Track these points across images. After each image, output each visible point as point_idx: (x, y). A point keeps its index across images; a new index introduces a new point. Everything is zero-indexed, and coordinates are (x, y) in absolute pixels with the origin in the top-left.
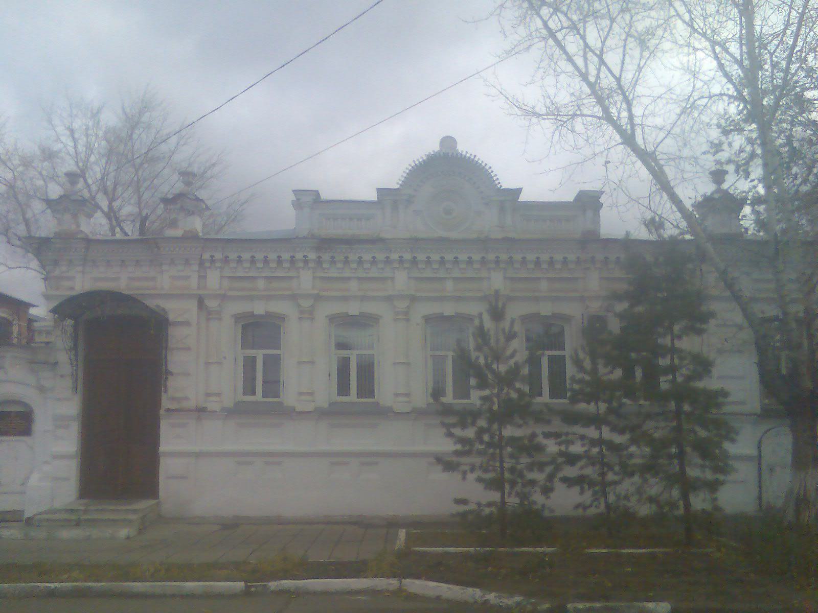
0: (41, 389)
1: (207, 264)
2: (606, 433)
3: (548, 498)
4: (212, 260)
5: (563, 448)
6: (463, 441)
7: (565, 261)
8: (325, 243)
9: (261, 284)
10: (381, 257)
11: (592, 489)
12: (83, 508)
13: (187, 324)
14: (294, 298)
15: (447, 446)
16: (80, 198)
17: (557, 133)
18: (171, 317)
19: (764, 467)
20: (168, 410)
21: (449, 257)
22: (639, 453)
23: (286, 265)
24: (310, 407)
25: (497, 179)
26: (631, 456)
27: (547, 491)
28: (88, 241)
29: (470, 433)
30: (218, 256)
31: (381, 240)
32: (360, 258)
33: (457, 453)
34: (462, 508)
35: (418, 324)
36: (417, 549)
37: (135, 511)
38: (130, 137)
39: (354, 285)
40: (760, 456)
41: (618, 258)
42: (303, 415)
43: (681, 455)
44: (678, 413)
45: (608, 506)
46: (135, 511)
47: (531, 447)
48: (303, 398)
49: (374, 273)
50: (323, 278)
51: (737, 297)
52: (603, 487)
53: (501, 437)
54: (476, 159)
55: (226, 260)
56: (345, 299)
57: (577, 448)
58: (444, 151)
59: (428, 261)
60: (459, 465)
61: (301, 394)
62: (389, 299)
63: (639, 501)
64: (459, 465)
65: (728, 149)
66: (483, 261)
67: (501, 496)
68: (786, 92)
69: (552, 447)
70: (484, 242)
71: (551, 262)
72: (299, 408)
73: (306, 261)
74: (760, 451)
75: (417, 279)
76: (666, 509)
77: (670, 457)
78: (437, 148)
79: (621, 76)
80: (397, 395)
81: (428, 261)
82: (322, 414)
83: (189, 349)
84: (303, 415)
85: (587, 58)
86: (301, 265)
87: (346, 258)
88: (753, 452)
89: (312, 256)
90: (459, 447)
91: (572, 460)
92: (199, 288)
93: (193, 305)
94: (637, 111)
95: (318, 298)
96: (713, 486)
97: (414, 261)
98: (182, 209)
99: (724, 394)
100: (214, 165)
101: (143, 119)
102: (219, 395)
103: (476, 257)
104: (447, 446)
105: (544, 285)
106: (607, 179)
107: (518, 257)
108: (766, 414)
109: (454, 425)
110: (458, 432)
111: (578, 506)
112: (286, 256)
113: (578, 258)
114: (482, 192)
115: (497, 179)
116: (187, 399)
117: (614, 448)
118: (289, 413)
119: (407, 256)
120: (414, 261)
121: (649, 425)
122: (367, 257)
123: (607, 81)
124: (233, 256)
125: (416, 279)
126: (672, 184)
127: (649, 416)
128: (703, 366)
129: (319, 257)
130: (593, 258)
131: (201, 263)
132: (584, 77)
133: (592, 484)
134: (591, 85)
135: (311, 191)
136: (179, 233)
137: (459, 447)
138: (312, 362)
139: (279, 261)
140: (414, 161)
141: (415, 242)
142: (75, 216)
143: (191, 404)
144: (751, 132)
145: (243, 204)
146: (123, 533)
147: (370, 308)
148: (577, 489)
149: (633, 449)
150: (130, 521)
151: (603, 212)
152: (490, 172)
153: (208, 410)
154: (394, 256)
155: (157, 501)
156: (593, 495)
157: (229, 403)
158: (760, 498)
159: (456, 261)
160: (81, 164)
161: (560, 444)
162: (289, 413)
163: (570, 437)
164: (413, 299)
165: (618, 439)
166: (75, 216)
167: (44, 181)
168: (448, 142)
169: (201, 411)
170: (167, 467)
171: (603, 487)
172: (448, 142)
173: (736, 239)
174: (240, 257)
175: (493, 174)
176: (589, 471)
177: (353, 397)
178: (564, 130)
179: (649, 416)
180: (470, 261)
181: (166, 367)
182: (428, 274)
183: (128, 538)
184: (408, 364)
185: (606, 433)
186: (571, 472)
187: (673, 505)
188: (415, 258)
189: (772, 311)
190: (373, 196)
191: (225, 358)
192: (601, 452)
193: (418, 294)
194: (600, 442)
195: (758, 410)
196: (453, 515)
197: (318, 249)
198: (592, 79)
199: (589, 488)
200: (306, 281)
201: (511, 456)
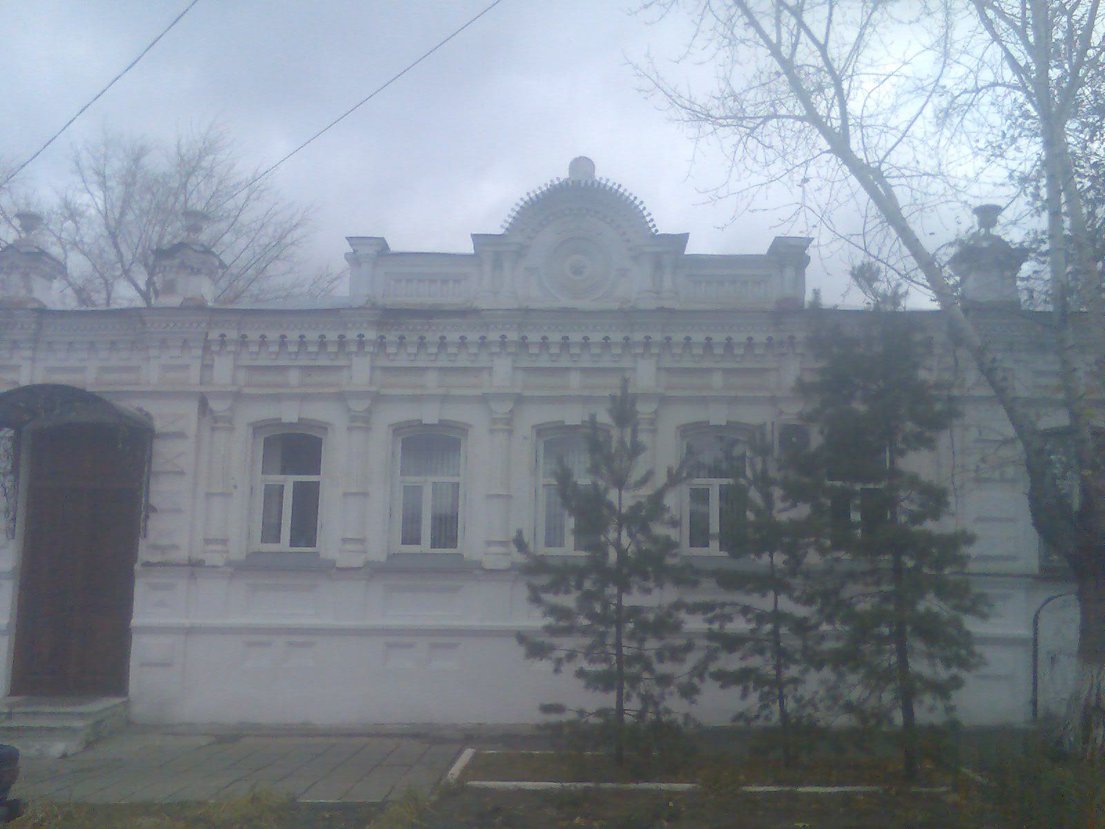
1: (215, 348)
2: (786, 604)
3: (693, 702)
4: (223, 341)
5: (716, 626)
6: (554, 611)
7: (750, 344)
8: (389, 316)
9: (294, 377)
10: (473, 336)
11: (759, 690)
12: (6, 710)
13: (181, 435)
14: (341, 397)
15: (534, 621)
16: (36, 250)
17: (741, 145)
18: (158, 425)
19: (1042, 656)
20: (147, 564)
21: (576, 337)
22: (833, 637)
23: (332, 349)
24: (358, 561)
25: (652, 220)
26: (823, 637)
27: (689, 692)
28: (43, 312)
29: (569, 601)
30: (232, 334)
31: (476, 312)
32: (443, 338)
33: (550, 630)
34: (554, 718)
35: (525, 438)
36: (476, 783)
37: (81, 716)
38: (184, 186)
39: (432, 379)
40: (1035, 640)
42: (347, 572)
43: (899, 638)
44: (898, 570)
45: (784, 715)
46: (81, 716)
47: (664, 625)
48: (349, 547)
49: (463, 361)
50: (386, 369)
51: (1001, 395)
52: (775, 687)
53: (619, 606)
54: (621, 190)
55: (243, 342)
56: (417, 399)
57: (739, 625)
58: (574, 179)
59: (544, 344)
60: (552, 648)
61: (345, 541)
62: (484, 399)
63: (828, 708)
64: (552, 648)
66: (627, 343)
67: (618, 695)
69: (695, 624)
70: (628, 315)
71: (729, 345)
72: (343, 562)
73: (361, 343)
74: (1036, 633)
75: (528, 370)
76: (872, 722)
77: (881, 639)
78: (564, 174)
79: (826, 42)
80: (489, 543)
81: (544, 344)
82: (374, 571)
83: (182, 473)
84: (347, 572)
85: (780, 21)
86: (354, 348)
87: (422, 338)
88: (1025, 632)
89: (371, 335)
90: (550, 620)
91: (731, 643)
92: (201, 384)
93: (190, 409)
94: (854, 107)
95: (378, 399)
96: (942, 690)
97: (523, 344)
98: (183, 266)
99: (970, 539)
100: (296, 226)
101: (204, 164)
102: (224, 541)
103: (617, 337)
104: (534, 621)
105: (717, 380)
106: (803, 205)
107: (678, 337)
108: (1047, 575)
109: (546, 589)
110: (550, 598)
111: (740, 716)
112: (332, 336)
113: (770, 339)
114: (628, 241)
115: (652, 220)
116: (175, 547)
117: (801, 626)
118: (329, 570)
119: (513, 336)
120: (523, 344)
121: (851, 590)
122: (453, 337)
123: (807, 55)
124: (253, 335)
125: (526, 370)
126: (905, 213)
127: (852, 576)
128: (935, 500)
129: (382, 337)
130: (792, 338)
131: (206, 348)
132: (775, 50)
133: (760, 681)
134: (782, 61)
135: (371, 238)
136: (174, 301)
137: (550, 620)
138: (365, 495)
139: (322, 344)
140: (528, 194)
141: (525, 315)
142: (26, 276)
143: (182, 555)
145: (336, 279)
146: (58, 748)
148: (736, 690)
149: (825, 627)
150: (74, 730)
151: (810, 271)
152: (642, 209)
153: (206, 564)
154: (494, 336)
155: (125, 699)
156: (761, 699)
157: (237, 551)
158: (1034, 703)
159: (586, 344)
160: (113, 224)
161: (711, 621)
162: (329, 570)
163: (727, 610)
164: (520, 400)
165: (801, 611)
166: (26, 276)
167: (63, 248)
168: (582, 164)
169: (194, 567)
170: (142, 648)
171: (775, 687)
172: (582, 164)
173: (1011, 310)
174: (263, 337)
176: (755, 662)
178: (752, 143)
179: (852, 576)
180: (606, 344)
181: (147, 500)
182: (544, 362)
183: (64, 756)
184: (508, 497)
185: (786, 604)
186: (731, 662)
187: (882, 716)
188: (524, 338)
189: (1060, 419)
190: (468, 248)
191: (235, 487)
192: (775, 633)
193: (527, 393)
194: (778, 617)
195: (1036, 571)
196: (538, 727)
197: (379, 325)
198: (785, 51)
199: (755, 689)
200: (360, 373)
201: (632, 636)
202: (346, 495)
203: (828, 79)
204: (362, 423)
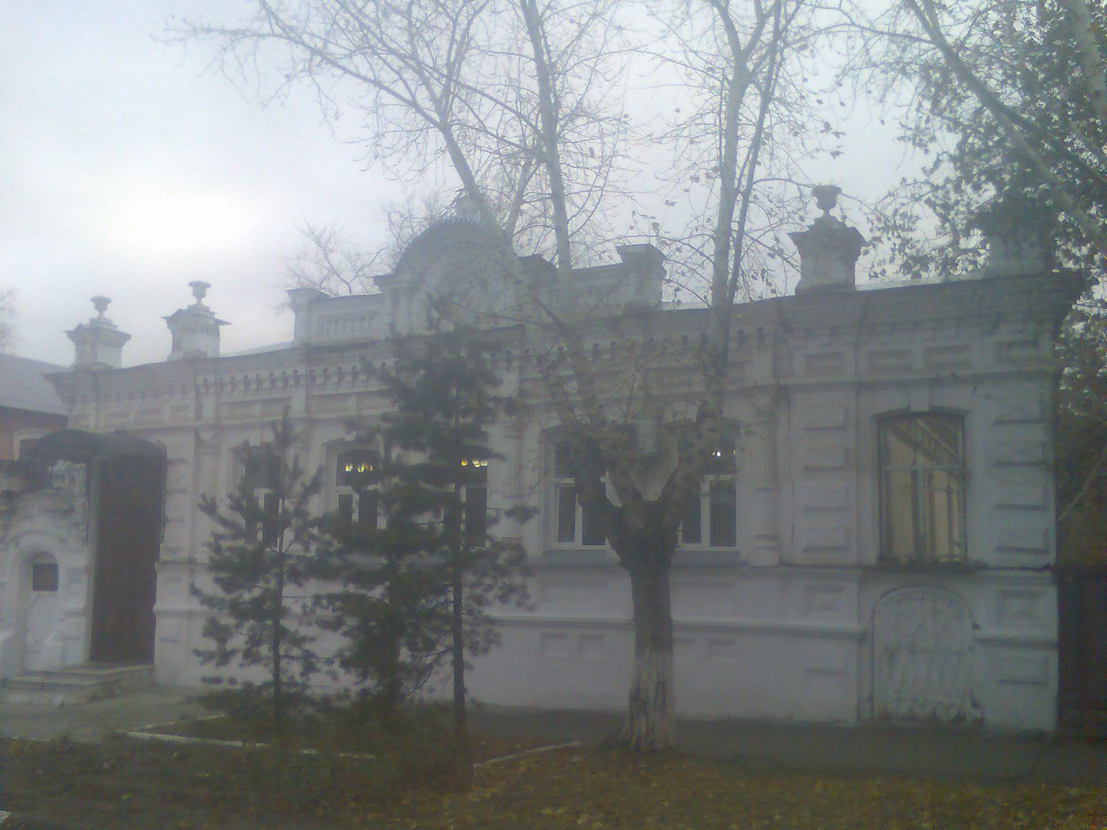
18: (171, 455)
20: (165, 562)
34: (216, 688)
41: (354, 368)
65: (767, 163)
113: (613, 344)
177: (578, 543)
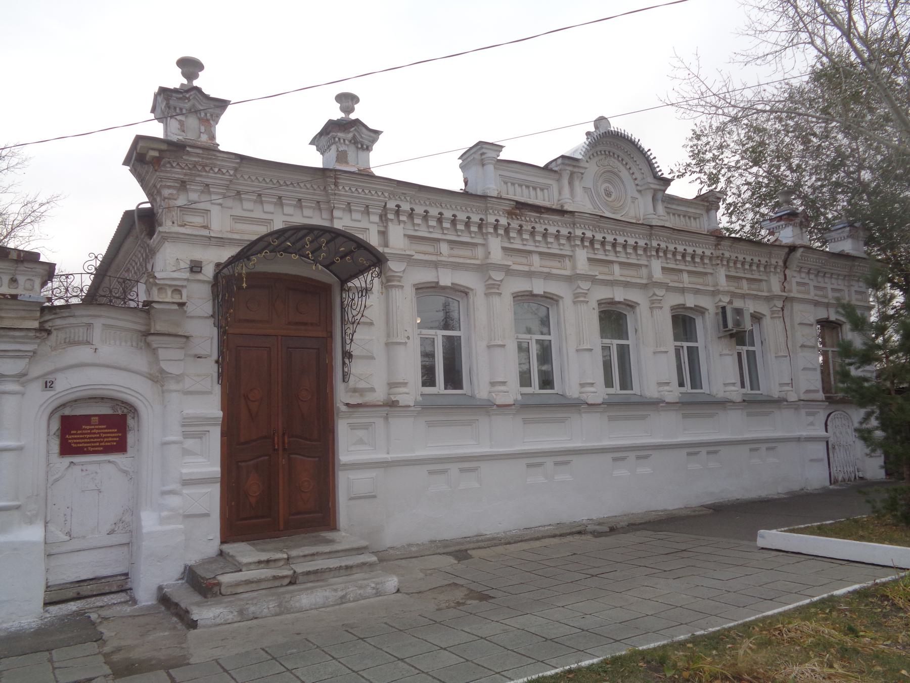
0: (159, 378)
19: (830, 446)
68: (829, 96)
75: (410, 237)
89: (503, 221)
116: (372, 390)
131: (383, 217)
144: (791, 218)
147: (553, 288)
175: (658, 169)
197: (510, 214)
202: (654, 353)
203: (806, 117)
204: (579, 298)
